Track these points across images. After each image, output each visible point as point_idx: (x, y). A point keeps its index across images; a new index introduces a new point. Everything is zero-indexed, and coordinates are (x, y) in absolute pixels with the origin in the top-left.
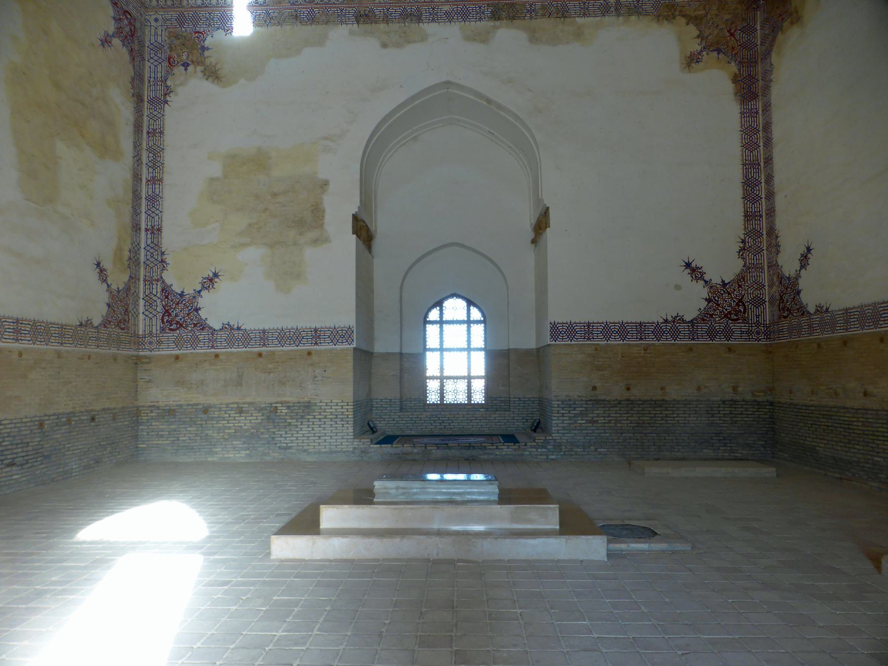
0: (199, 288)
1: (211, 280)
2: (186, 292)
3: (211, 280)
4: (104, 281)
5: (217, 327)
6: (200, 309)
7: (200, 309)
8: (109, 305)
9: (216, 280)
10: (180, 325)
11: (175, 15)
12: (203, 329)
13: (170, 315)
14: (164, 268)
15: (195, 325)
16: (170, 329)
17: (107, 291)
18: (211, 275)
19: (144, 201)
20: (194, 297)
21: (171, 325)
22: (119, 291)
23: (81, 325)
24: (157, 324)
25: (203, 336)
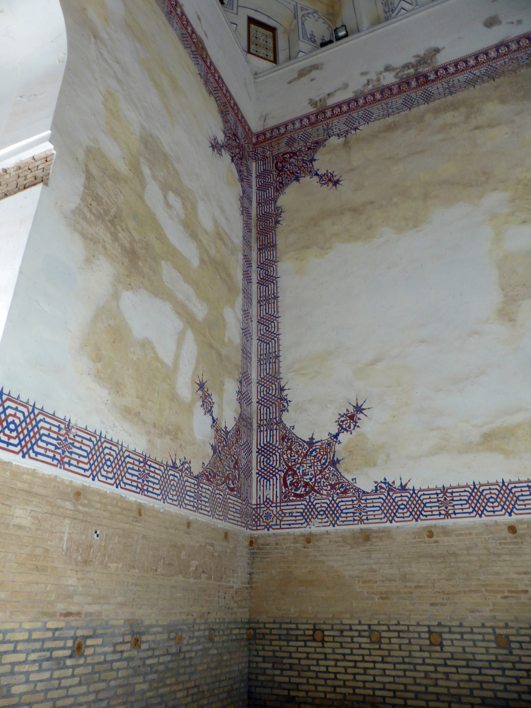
0: (334, 431)
1: (352, 417)
2: (317, 438)
3: (352, 417)
4: (210, 411)
5: (279, 204)
6: (338, 461)
7: (338, 461)
8: (214, 448)
9: (360, 416)
10: (310, 488)
11: (503, 61)
12: (345, 492)
13: (295, 473)
14: (284, 409)
15: (333, 487)
16: (296, 495)
17: (212, 426)
18: (351, 409)
19: (254, 454)
20: (329, 444)
21: (297, 489)
22: (227, 433)
23: (174, 466)
24: (273, 490)
25: (346, 503)
